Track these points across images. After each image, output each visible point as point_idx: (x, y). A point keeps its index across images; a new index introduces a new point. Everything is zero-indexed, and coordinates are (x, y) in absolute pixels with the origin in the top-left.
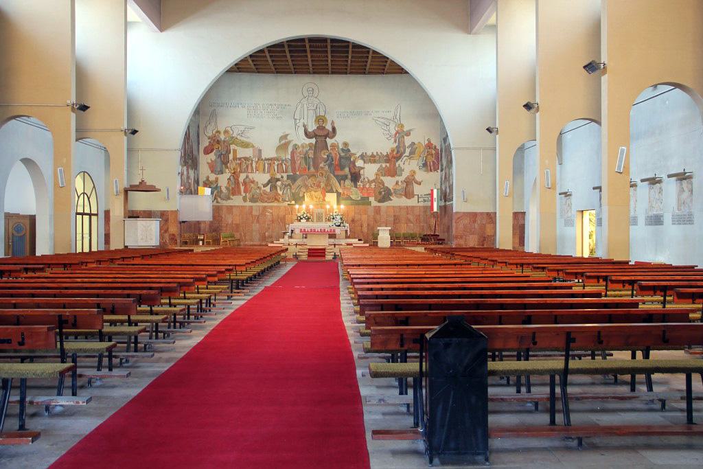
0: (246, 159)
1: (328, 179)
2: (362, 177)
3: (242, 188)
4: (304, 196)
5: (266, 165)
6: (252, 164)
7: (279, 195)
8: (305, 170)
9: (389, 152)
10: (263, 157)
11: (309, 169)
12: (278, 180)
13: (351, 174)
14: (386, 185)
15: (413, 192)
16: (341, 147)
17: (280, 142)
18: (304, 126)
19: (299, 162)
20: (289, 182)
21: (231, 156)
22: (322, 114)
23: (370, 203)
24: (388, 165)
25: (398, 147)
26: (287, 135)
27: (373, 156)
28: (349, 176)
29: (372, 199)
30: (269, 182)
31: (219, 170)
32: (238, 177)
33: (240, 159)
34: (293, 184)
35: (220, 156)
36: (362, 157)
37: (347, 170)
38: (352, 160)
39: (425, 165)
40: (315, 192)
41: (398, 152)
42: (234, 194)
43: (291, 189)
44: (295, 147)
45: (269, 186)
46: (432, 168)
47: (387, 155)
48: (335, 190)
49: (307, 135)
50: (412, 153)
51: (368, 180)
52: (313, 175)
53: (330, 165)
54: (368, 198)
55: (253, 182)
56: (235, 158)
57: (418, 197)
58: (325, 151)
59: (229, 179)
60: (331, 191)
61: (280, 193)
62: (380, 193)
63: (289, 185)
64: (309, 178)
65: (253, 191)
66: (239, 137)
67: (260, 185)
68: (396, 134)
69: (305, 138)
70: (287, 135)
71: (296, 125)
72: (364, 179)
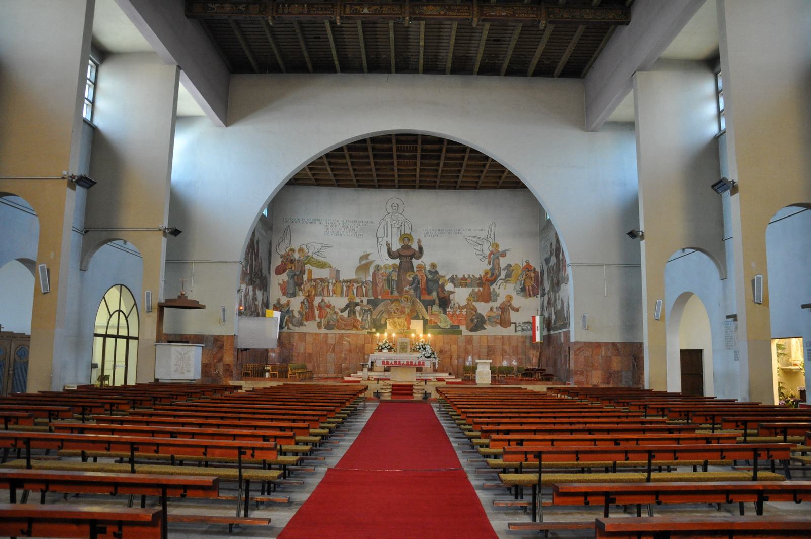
0: (322, 280)
1: (413, 303)
2: (452, 302)
3: (317, 313)
4: (386, 323)
5: (345, 288)
6: (328, 286)
7: (359, 321)
8: (389, 294)
9: (482, 274)
10: (341, 279)
11: (392, 292)
12: (357, 304)
13: (440, 299)
14: (479, 311)
15: (510, 319)
16: (428, 268)
17: (360, 262)
18: (388, 245)
19: (381, 284)
20: (370, 307)
21: (305, 277)
22: (408, 232)
23: (460, 332)
24: (481, 289)
25: (492, 269)
26: (368, 255)
27: (464, 279)
28: (437, 302)
29: (463, 328)
30: (347, 306)
31: (291, 292)
32: (313, 300)
33: (315, 280)
34: (374, 309)
35: (293, 277)
36: (452, 280)
37: (435, 294)
38: (440, 283)
39: (523, 289)
40: (399, 318)
41: (492, 275)
42: (307, 320)
43: (371, 314)
44: (378, 268)
45: (347, 312)
46: (531, 293)
47: (480, 279)
48: (421, 318)
49: (391, 254)
50: (508, 276)
51: (459, 306)
52: (397, 300)
53: (416, 289)
54: (458, 326)
55: (329, 306)
56: (310, 280)
57: (516, 326)
58: (410, 273)
59: (302, 303)
60: (417, 318)
61: (360, 319)
62: (472, 320)
63: (369, 310)
64: (392, 303)
65: (329, 316)
66: (314, 256)
67: (337, 310)
68: (490, 255)
69: (388, 257)
70: (368, 255)
71: (378, 243)
72: (454, 304)
